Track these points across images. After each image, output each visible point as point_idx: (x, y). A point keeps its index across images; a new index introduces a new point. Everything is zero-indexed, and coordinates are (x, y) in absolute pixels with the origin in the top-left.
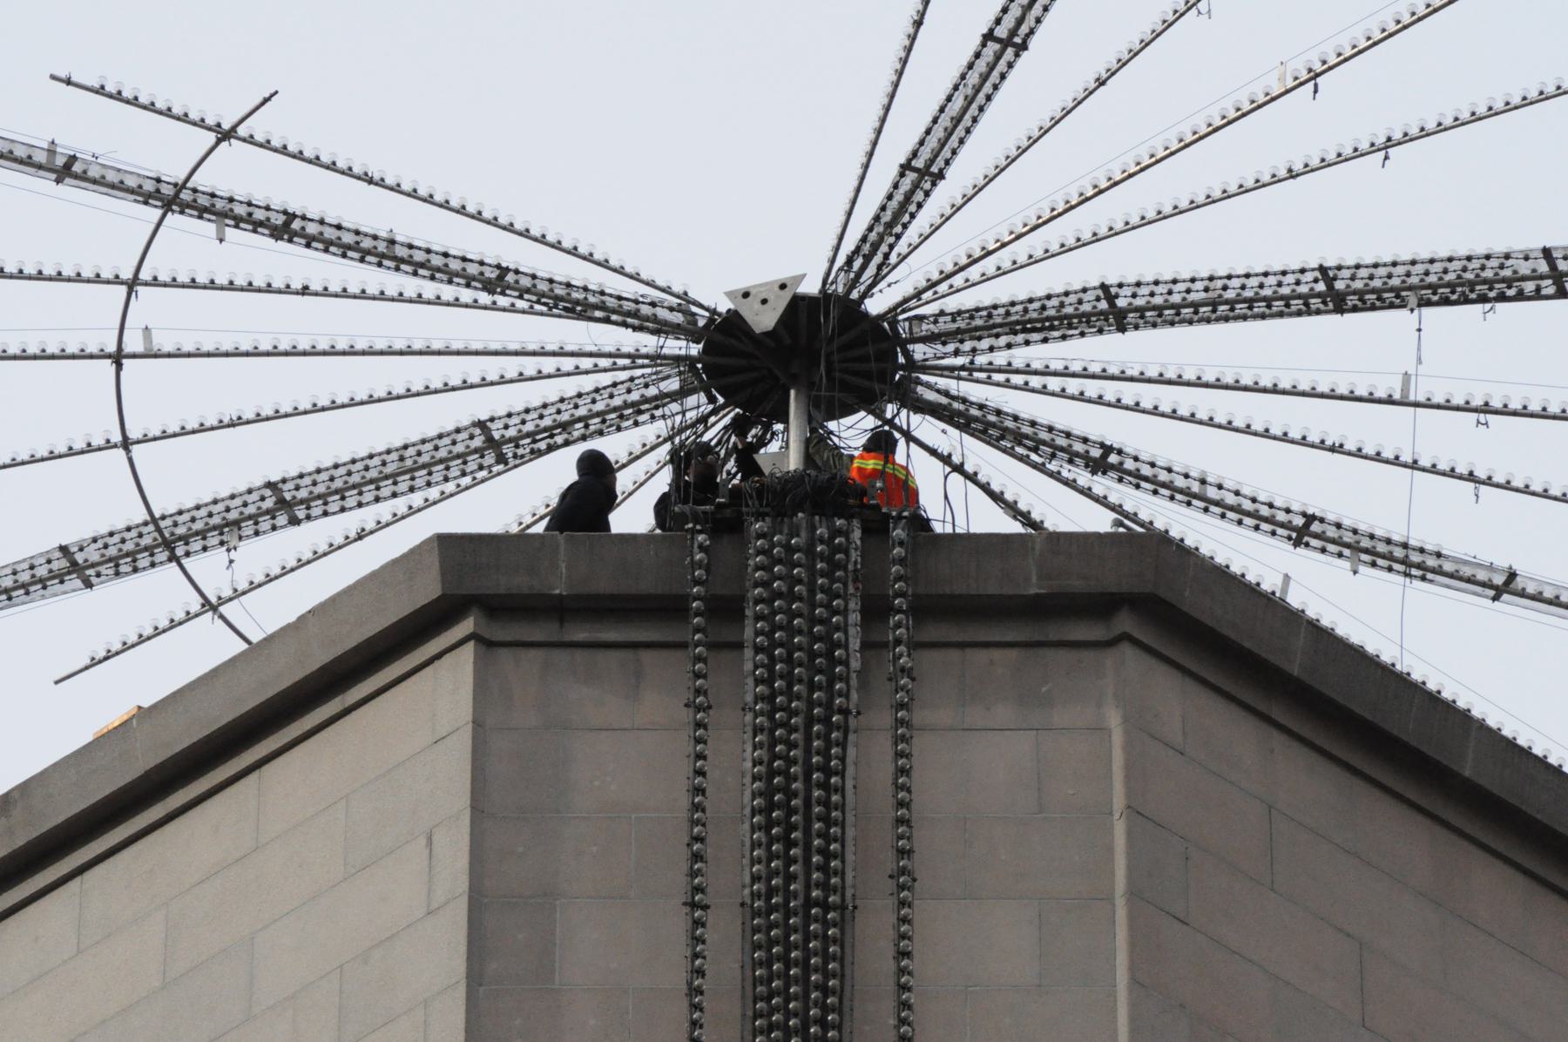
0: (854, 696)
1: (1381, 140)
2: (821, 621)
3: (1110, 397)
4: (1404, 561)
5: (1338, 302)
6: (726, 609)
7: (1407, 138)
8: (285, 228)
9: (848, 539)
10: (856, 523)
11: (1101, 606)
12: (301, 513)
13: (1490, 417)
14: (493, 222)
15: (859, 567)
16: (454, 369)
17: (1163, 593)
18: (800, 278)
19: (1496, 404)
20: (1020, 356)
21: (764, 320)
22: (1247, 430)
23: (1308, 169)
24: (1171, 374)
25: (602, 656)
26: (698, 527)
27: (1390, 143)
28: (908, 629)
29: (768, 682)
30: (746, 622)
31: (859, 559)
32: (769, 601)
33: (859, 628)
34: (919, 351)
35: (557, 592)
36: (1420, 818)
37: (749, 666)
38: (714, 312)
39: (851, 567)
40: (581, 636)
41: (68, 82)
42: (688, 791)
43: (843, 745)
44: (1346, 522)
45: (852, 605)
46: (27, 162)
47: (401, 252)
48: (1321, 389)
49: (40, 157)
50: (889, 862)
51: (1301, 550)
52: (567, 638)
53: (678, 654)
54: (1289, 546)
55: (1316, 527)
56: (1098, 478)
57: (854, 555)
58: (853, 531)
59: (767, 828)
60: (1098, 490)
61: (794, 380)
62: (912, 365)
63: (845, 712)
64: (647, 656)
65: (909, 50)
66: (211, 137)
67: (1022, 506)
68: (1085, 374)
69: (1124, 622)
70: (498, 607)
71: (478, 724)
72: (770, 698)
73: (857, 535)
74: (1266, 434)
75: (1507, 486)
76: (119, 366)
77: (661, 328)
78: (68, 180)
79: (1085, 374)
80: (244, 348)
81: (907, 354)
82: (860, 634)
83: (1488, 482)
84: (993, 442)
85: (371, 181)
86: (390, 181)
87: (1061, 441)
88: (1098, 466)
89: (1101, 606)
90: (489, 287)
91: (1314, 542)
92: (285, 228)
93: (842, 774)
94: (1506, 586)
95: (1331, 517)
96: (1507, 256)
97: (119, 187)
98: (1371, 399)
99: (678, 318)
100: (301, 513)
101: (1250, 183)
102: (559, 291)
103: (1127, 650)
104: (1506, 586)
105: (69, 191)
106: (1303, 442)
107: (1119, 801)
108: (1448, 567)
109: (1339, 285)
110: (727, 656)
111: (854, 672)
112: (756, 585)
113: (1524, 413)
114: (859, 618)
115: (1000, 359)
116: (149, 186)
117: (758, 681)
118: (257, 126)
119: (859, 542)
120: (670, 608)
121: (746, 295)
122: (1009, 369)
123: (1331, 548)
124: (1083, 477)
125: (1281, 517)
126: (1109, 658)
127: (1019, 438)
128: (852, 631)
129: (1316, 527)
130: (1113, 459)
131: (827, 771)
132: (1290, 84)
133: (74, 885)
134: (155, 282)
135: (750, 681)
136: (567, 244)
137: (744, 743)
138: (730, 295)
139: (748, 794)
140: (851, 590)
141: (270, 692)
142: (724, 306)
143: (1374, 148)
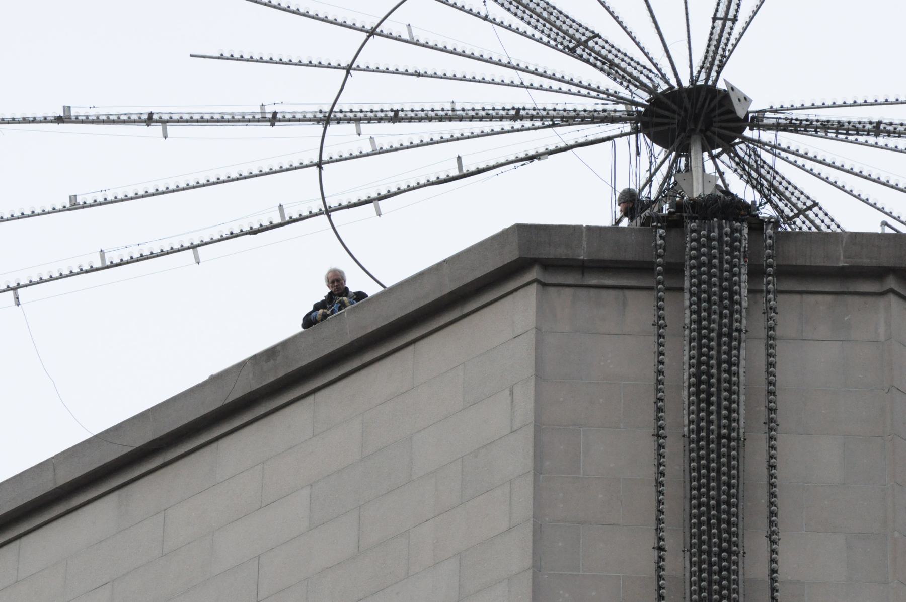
0: (744, 321)
2: (726, 280)
9: (741, 234)
15: (747, 249)
26: (659, 225)
28: (774, 285)
30: (685, 278)
31: (747, 246)
32: (698, 268)
33: (746, 284)
35: (582, 257)
39: (742, 250)
40: (594, 282)
43: (738, 349)
45: (743, 271)
46: (254, 120)
57: (744, 243)
58: (744, 229)
63: (739, 330)
78: (276, 124)
82: (747, 288)
84: (796, 131)
93: (738, 365)
111: (745, 308)
114: (747, 278)
119: (747, 236)
120: (642, 268)
128: (743, 285)
131: (731, 364)
135: (687, 312)
140: (742, 262)
141: (422, 303)
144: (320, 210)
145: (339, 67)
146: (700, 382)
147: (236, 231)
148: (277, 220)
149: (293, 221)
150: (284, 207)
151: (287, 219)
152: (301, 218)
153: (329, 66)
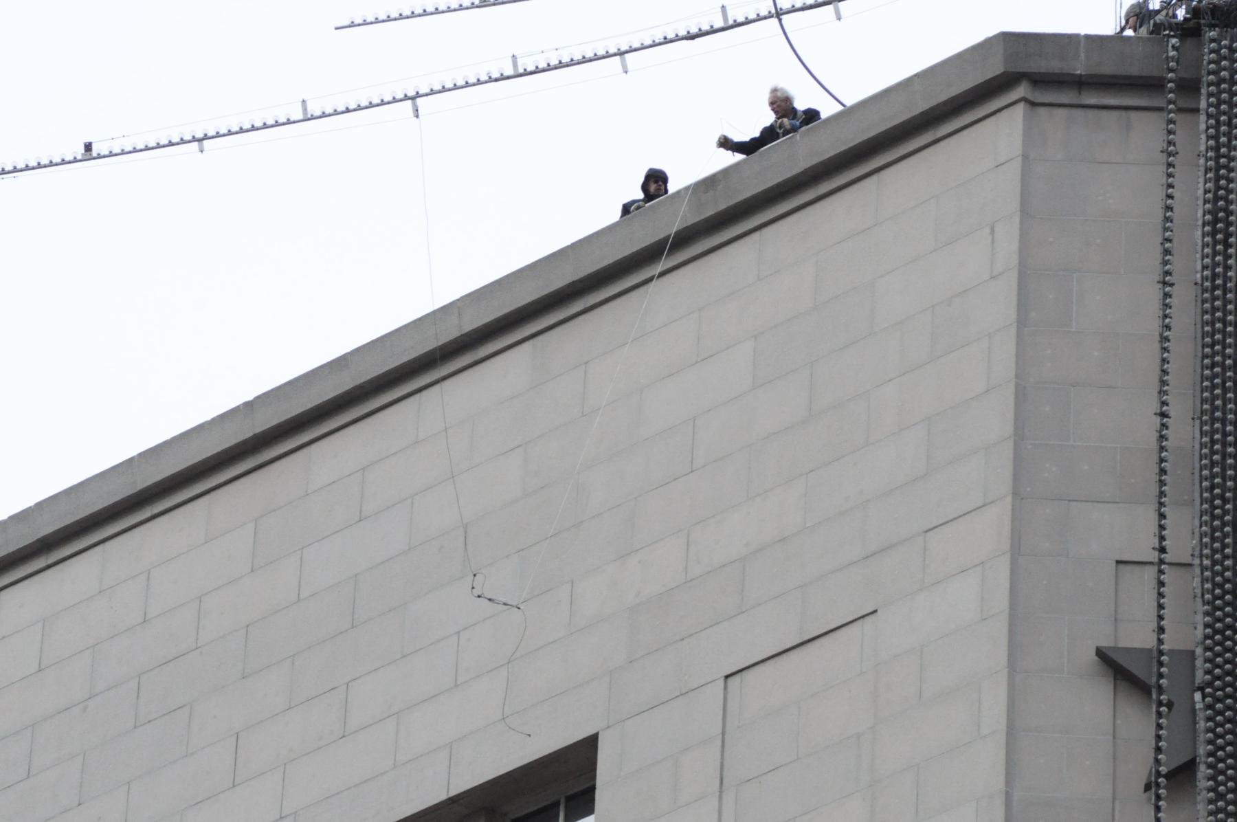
6: (1189, 87)
25: (1104, 113)
26: (1172, 33)
30: (1202, 98)
35: (1079, 72)
40: (1092, 101)
42: (1162, 208)
64: (1134, 115)
70: (1040, 81)
71: (1025, 157)
117: (1209, 138)
120: (1151, 85)
133: (756, 236)
137: (1199, 177)
139: (1200, 213)
144: (770, 12)
146: (1216, 221)
147: (671, 36)
148: (719, 23)
149: (737, 25)
150: (727, 8)
151: (731, 22)
152: (747, 22)
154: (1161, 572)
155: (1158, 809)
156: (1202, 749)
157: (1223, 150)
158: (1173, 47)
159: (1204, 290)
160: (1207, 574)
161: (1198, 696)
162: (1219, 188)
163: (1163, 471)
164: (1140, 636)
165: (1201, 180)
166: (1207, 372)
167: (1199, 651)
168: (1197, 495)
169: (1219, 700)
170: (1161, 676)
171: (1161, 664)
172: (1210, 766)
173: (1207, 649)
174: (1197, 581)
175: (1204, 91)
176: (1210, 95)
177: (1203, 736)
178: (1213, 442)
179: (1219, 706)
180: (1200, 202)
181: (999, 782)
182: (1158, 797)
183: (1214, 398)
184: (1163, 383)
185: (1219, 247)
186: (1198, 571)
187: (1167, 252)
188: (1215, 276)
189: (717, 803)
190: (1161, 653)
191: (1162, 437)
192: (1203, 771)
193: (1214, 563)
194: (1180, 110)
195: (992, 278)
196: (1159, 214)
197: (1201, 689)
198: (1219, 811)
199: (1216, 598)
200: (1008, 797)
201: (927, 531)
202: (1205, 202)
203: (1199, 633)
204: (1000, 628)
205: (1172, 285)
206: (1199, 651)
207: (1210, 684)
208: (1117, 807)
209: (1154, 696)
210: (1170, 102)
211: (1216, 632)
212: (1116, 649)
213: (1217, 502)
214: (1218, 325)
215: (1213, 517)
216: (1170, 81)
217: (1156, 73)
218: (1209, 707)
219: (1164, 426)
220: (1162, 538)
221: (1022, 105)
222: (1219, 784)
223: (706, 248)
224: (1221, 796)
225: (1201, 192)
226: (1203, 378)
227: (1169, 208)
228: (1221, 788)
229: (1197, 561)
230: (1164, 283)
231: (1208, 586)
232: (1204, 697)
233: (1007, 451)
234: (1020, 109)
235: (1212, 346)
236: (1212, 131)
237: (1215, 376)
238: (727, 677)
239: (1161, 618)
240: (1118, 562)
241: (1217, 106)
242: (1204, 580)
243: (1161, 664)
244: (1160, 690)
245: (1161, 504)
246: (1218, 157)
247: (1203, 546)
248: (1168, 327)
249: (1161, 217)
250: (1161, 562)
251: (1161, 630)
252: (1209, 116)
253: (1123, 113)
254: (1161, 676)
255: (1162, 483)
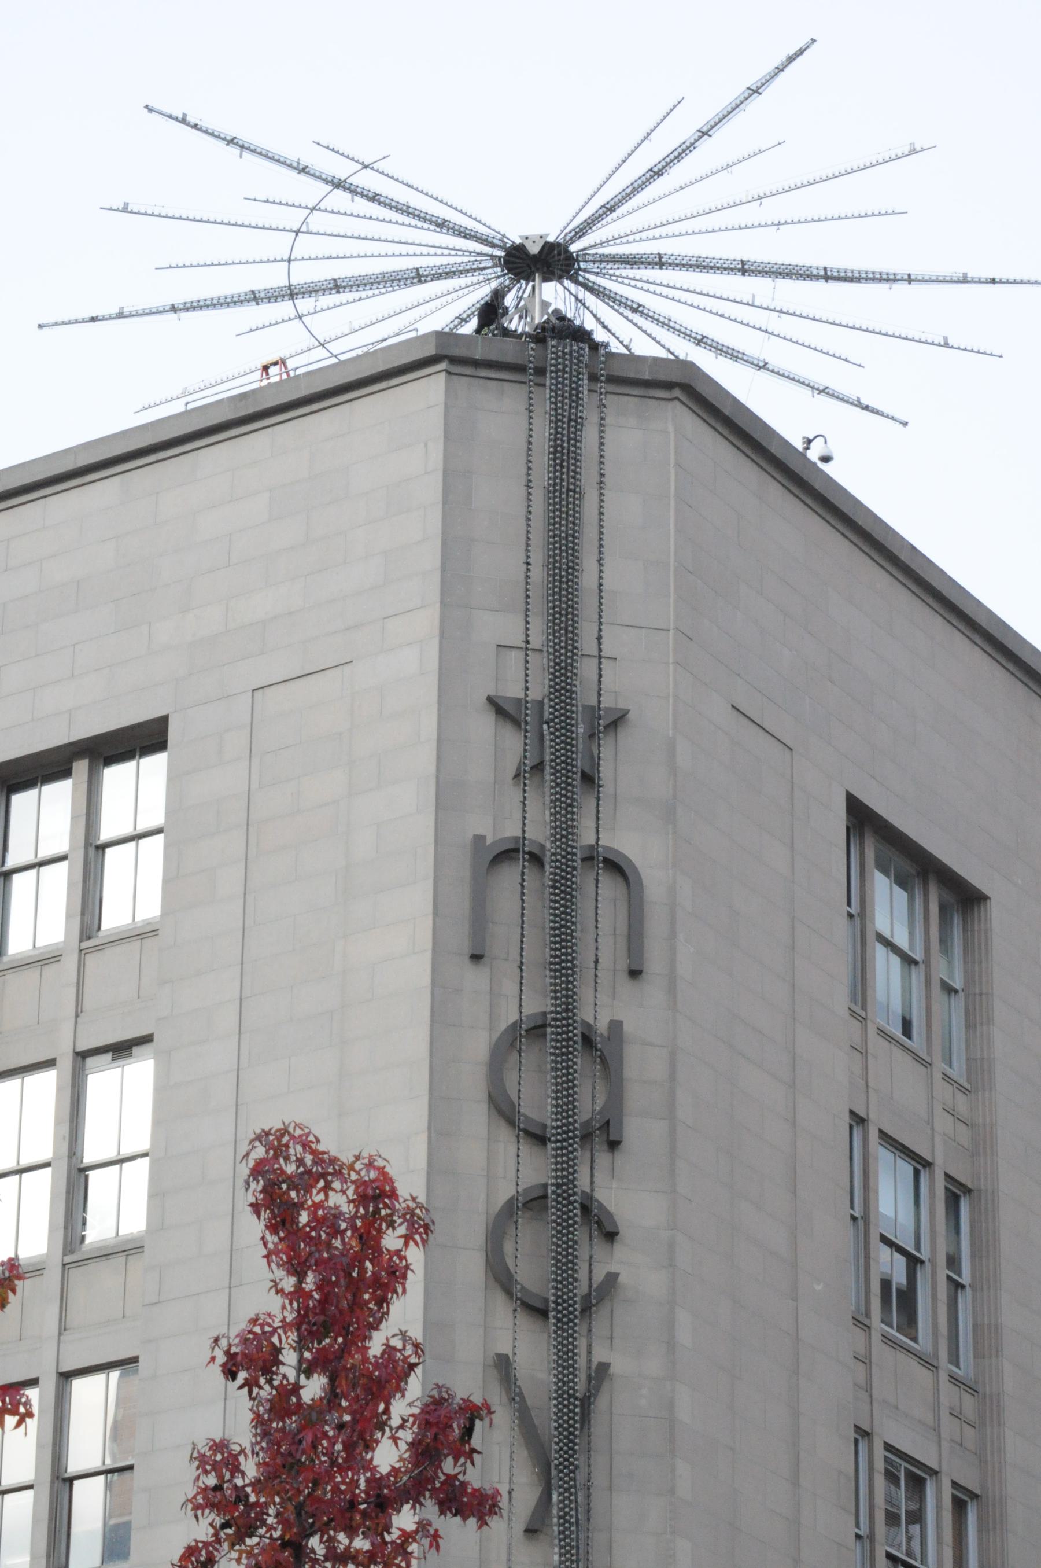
1: (776, 222)
3: (651, 290)
4: (732, 355)
5: (744, 271)
6: (540, 371)
7: (786, 223)
8: (374, 198)
10: (587, 345)
11: (669, 386)
12: (341, 290)
13: (782, 315)
14: (446, 204)
16: (411, 249)
17: (692, 384)
18: (547, 235)
19: (785, 310)
20: (624, 273)
21: (534, 249)
22: (698, 308)
23: (746, 227)
24: (671, 284)
25: (489, 382)
27: (779, 224)
29: (555, 403)
34: (582, 265)
36: (755, 466)
37: (548, 396)
38: (513, 242)
41: (318, 144)
44: (715, 339)
46: (290, 166)
47: (410, 210)
48: (724, 297)
49: (295, 165)
50: (597, 479)
51: (698, 347)
52: (478, 374)
53: (523, 386)
54: (693, 345)
55: (705, 340)
56: (634, 315)
59: (554, 460)
60: (630, 317)
61: (538, 270)
62: (580, 269)
64: (506, 385)
65: (617, 169)
66: (360, 166)
67: (602, 320)
68: (647, 282)
69: (677, 393)
70: (454, 360)
71: (446, 404)
72: (556, 410)
73: (587, 350)
74: (704, 310)
75: (778, 336)
76: (297, 235)
77: (493, 246)
79: (647, 282)
80: (342, 234)
81: (579, 265)
83: (772, 334)
85: (409, 186)
86: (415, 187)
87: (624, 301)
88: (635, 311)
89: (669, 386)
90: (438, 225)
91: (702, 345)
92: (374, 198)
94: (763, 366)
95: (711, 337)
96: (811, 267)
97: (319, 178)
98: (741, 303)
99: (500, 243)
100: (341, 290)
101: (667, 193)
102: (462, 229)
103: (677, 402)
104: (763, 366)
105: (303, 177)
106: (710, 312)
107: (672, 461)
108: (745, 358)
109: (746, 267)
110: (541, 389)
112: (552, 365)
113: (794, 314)
115: (618, 273)
116: (330, 179)
117: (551, 403)
118: (380, 166)
121: (527, 238)
122: (620, 276)
123: (708, 347)
124: (627, 313)
125: (694, 335)
126: (670, 404)
127: (609, 297)
129: (705, 340)
130: (641, 309)
132: (750, 199)
133: (270, 430)
134: (296, 260)
136: (469, 214)
138: (521, 237)
139: (547, 447)
142: (518, 241)
143: (773, 224)
145: (282, 260)
153: (352, 257)
154: (527, 655)
155: (525, 791)
156: (548, 757)
157: (559, 411)
158: (532, 348)
159: (549, 492)
160: (551, 657)
161: (545, 727)
162: (557, 433)
163: (528, 597)
164: (513, 690)
165: (547, 427)
166: (551, 540)
167: (546, 701)
168: (545, 611)
169: (557, 730)
170: (527, 715)
171: (527, 708)
172: (552, 767)
173: (551, 700)
174: (545, 661)
175: (548, 375)
176: (552, 378)
177: (548, 751)
178: (554, 581)
179: (557, 733)
180: (547, 440)
181: (432, 769)
182: (525, 785)
183: (555, 555)
184: (528, 545)
185: (558, 468)
186: (546, 654)
187: (529, 468)
188: (555, 485)
189: (248, 763)
190: (527, 702)
191: (528, 577)
192: (548, 770)
193: (556, 651)
194: (536, 384)
195: (426, 473)
196: (525, 446)
197: (547, 723)
198: (557, 793)
199: (556, 671)
200: (437, 777)
201: (385, 618)
202: (550, 440)
203: (546, 691)
204: (433, 680)
205: (531, 488)
206: (546, 701)
207: (552, 720)
208: (497, 787)
209: (523, 726)
210: (530, 381)
211: (556, 691)
212: (496, 696)
213: (557, 616)
214: (557, 513)
215: (555, 624)
216: (530, 368)
217: (520, 362)
218: (552, 733)
219: (528, 570)
220: (527, 635)
221: (444, 374)
222: (557, 778)
223: (237, 434)
224: (558, 785)
225: (547, 434)
226: (549, 543)
227: (530, 443)
228: (558, 780)
229: (545, 649)
230: (528, 486)
231: (552, 664)
232: (549, 727)
233: (437, 578)
234: (444, 374)
235: (554, 525)
236: (553, 399)
237: (555, 542)
238: (254, 690)
239: (527, 681)
240: (498, 646)
241: (556, 385)
242: (549, 660)
243: (527, 708)
244: (526, 723)
245: (527, 616)
246: (557, 415)
247: (548, 640)
248: (530, 513)
249: (526, 448)
250: (527, 649)
251: (527, 689)
252: (551, 390)
253: (500, 383)
254: (527, 715)
255: (527, 603)
